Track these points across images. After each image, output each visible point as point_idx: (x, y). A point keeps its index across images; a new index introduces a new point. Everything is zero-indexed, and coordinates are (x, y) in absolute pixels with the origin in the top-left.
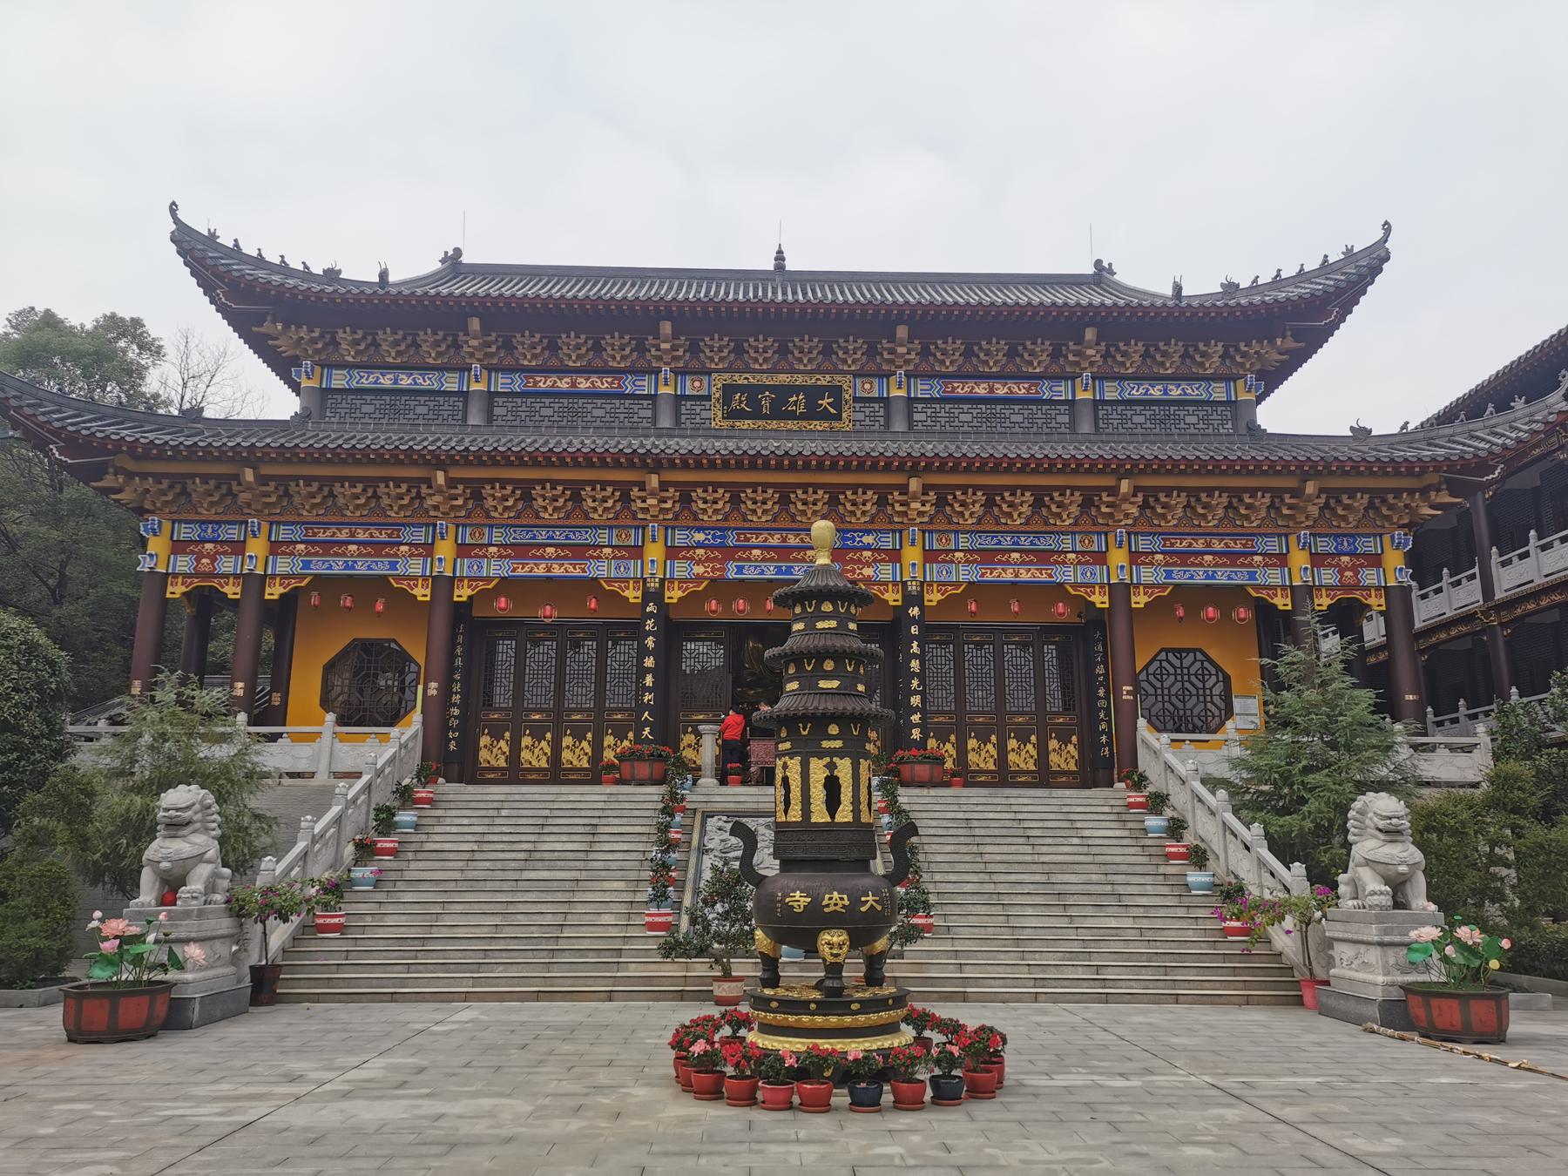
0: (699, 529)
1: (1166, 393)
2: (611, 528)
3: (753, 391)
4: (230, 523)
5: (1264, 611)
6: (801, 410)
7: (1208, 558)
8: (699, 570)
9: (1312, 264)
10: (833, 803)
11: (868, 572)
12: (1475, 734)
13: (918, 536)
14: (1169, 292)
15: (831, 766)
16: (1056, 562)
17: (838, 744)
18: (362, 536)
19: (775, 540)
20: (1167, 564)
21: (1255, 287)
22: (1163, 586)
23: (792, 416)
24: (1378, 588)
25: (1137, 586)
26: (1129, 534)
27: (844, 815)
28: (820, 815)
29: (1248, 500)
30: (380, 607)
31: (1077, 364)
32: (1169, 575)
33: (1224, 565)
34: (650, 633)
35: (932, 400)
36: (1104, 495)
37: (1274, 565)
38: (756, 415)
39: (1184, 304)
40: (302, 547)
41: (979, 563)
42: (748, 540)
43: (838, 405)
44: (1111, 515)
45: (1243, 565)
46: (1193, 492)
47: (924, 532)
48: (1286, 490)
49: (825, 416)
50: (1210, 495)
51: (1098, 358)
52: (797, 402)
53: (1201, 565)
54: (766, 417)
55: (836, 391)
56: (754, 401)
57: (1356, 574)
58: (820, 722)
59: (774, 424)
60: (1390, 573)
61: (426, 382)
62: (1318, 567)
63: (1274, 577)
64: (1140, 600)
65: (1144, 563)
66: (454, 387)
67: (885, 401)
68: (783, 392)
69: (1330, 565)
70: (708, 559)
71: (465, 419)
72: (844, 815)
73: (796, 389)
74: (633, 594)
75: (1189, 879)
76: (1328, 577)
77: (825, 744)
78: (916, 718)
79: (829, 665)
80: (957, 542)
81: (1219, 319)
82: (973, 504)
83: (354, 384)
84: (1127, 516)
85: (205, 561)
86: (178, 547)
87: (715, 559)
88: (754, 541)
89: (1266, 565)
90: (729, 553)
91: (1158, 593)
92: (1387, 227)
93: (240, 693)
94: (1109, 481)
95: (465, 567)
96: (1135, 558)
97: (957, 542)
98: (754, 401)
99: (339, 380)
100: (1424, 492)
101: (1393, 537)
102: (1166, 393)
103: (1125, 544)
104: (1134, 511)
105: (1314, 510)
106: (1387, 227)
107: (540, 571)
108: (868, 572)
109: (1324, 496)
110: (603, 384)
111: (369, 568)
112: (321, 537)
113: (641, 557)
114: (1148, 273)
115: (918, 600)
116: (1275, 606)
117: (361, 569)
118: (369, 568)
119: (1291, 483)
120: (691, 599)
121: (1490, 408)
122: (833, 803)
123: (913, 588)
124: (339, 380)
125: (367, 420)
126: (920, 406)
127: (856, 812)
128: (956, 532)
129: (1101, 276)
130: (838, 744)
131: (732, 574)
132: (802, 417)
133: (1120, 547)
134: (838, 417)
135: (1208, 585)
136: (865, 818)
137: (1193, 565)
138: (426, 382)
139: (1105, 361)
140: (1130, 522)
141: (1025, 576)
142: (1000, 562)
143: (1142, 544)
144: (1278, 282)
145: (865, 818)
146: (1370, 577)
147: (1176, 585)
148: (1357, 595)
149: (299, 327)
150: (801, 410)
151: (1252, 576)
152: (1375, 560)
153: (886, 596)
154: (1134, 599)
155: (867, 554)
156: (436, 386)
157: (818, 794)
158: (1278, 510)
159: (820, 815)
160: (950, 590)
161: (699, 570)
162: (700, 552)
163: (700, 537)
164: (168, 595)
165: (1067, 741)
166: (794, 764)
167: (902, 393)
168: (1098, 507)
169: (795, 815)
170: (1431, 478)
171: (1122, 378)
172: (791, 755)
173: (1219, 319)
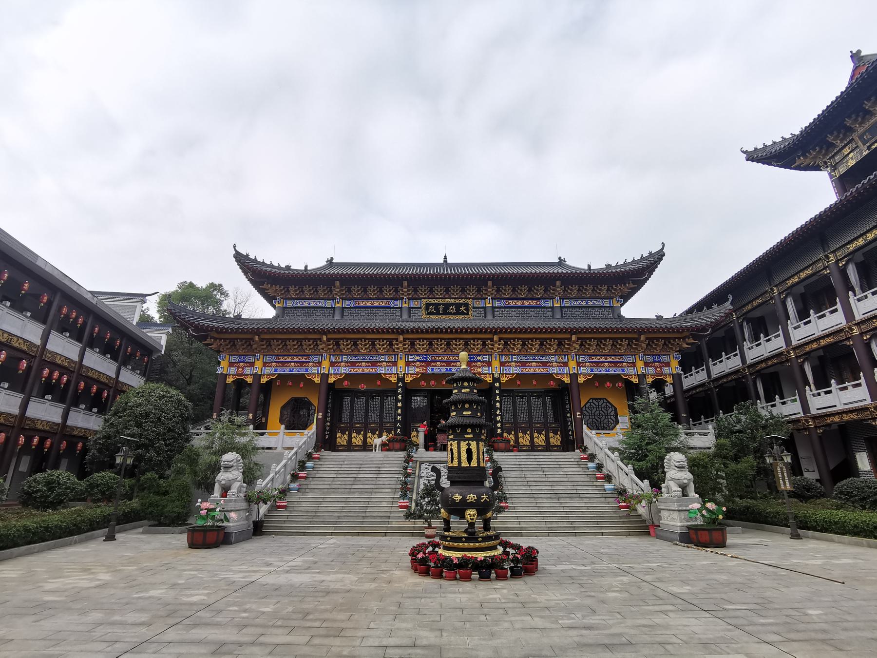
0: (418, 355)
3: (436, 305)
5: (628, 383)
6: (454, 311)
8: (417, 370)
9: (638, 257)
10: (469, 459)
15: (469, 445)
17: (471, 436)
19: (445, 359)
21: (617, 266)
23: (451, 314)
27: (474, 463)
28: (465, 464)
30: (302, 385)
32: (592, 370)
38: (438, 313)
43: (467, 309)
46: (599, 340)
49: (463, 313)
52: (453, 309)
55: (466, 305)
56: (437, 309)
58: (464, 427)
63: (631, 371)
64: (581, 380)
68: (447, 306)
72: (474, 463)
76: (651, 370)
77: (466, 436)
79: (467, 406)
88: (437, 359)
90: (428, 364)
91: (588, 377)
92: (663, 245)
94: (568, 336)
96: (579, 364)
98: (437, 309)
99: (290, 304)
100: (684, 338)
104: (578, 347)
105: (644, 346)
106: (663, 245)
114: (578, 261)
115: (498, 380)
117: (295, 372)
119: (635, 336)
122: (469, 459)
124: (290, 304)
127: (479, 462)
130: (471, 436)
131: (430, 372)
132: (454, 314)
134: (467, 314)
136: (482, 465)
141: (538, 371)
143: (581, 359)
145: (482, 465)
148: (243, 377)
150: (454, 311)
151: (623, 370)
157: (464, 455)
159: (465, 464)
161: (417, 370)
163: (418, 358)
166: (455, 444)
169: (455, 464)
170: (686, 334)
172: (472, 439)
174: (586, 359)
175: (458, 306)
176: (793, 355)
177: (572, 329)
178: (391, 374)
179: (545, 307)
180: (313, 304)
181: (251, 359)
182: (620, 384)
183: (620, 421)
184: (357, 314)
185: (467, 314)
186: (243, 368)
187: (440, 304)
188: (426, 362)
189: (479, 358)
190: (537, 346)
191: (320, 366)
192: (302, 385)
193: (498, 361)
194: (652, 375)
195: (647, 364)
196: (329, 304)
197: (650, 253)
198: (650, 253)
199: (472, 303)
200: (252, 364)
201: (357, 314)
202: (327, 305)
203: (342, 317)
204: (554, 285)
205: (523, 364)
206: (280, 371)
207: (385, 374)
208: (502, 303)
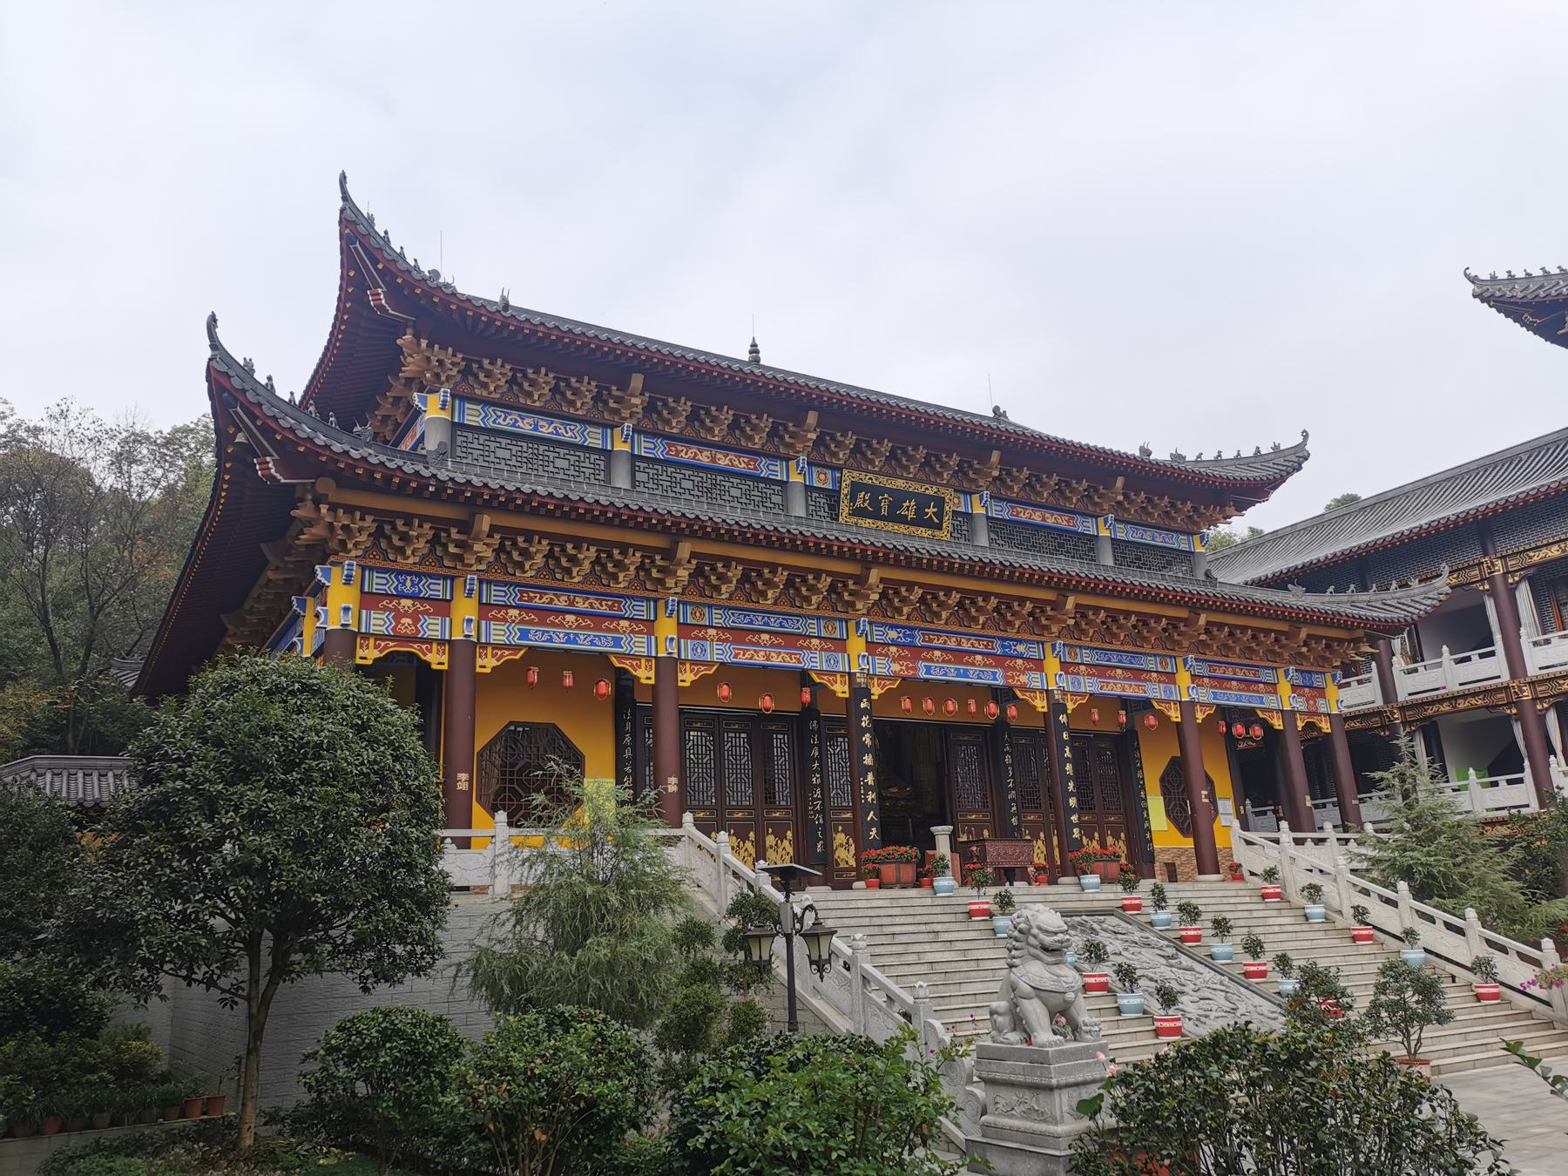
0: (892, 627)
1: (536, 429)
2: (818, 618)
3: (876, 491)
4: (431, 576)
5: (624, 683)
6: (911, 515)
7: (570, 618)
8: (896, 667)
9: (1248, 452)
11: (1023, 679)
12: (680, 825)
13: (356, 572)
14: (745, 356)
16: (802, 648)
18: (581, 605)
19: (952, 644)
20: (522, 622)
21: (1199, 460)
22: (515, 648)
23: (903, 520)
24: (441, 642)
25: (484, 646)
26: (481, 582)
29: (401, 528)
30: (568, 682)
31: (616, 412)
32: (524, 634)
33: (587, 628)
34: (866, 730)
35: (656, 461)
36: (454, 531)
37: (641, 632)
38: (876, 515)
39: (508, 314)
40: (515, 612)
41: (733, 642)
42: (931, 641)
43: (940, 515)
44: (460, 558)
45: (608, 630)
46: (558, 540)
47: (363, 569)
48: (850, 576)
49: (929, 524)
50: (408, 524)
51: (639, 410)
52: (909, 509)
53: (562, 626)
54: (883, 518)
55: (940, 502)
56: (875, 502)
57: (416, 621)
59: (890, 526)
60: (1184, 691)
61: (570, 433)
62: (369, 608)
63: (639, 645)
64: (487, 663)
65: (495, 619)
66: (598, 444)
67: (607, 454)
68: (899, 497)
69: (385, 609)
70: (900, 658)
71: (608, 479)
73: (908, 495)
74: (841, 689)
75: (1215, 950)
76: (379, 622)
78: (1074, 818)
80: (711, 619)
81: (707, 378)
82: (360, 530)
83: (491, 425)
84: (480, 560)
85: (404, 620)
86: (369, 600)
87: (905, 658)
88: (936, 643)
89: (633, 632)
90: (915, 652)
91: (508, 655)
92: (1305, 435)
93: (673, 788)
94: (1183, 613)
95: (688, 650)
96: (485, 609)
97: (711, 619)
98: (875, 502)
99: (473, 415)
101: (858, 624)
102: (536, 429)
103: (475, 594)
104: (489, 554)
105: (683, 574)
106: (1305, 435)
107: (760, 659)
108: (1023, 679)
109: (497, 536)
110: (741, 464)
111: (593, 644)
112: (537, 602)
113: (844, 651)
114: (1365, 493)
115: (866, 693)
116: (834, 692)
117: (583, 645)
118: (928, 672)
119: (1183, 613)
120: (703, 684)
121: (1394, 585)
123: (861, 680)
124: (473, 415)
125: (735, 504)
126: (642, 465)
128: (710, 606)
129: (435, 274)
131: (922, 675)
132: (913, 523)
133: (469, 595)
134: (940, 528)
135: (566, 650)
137: (553, 624)
138: (570, 433)
139: (510, 389)
140: (483, 567)
141: (776, 661)
142: (751, 643)
143: (495, 595)
144: (1218, 460)
146: (433, 627)
147: (530, 647)
148: (414, 648)
149: (444, 348)
150: (911, 515)
151: (617, 642)
152: (442, 607)
153: (429, 658)
154: (479, 662)
155: (1020, 662)
156: (579, 440)
158: (648, 572)
160: (704, 671)
161: (896, 667)
162: (893, 649)
163: (893, 634)
164: (479, 670)
165: (783, 837)
167: (626, 448)
168: (445, 546)
170: (1360, 633)
171: (486, 402)
173: (707, 378)
174: (512, 597)
175: (922, 501)
176: (1527, 695)
177: (477, 493)
178: (1168, 702)
179: (767, 480)
180: (546, 430)
181: (1035, 653)
182: (605, 688)
183: (1221, 810)
184: (674, 483)
185: (940, 528)
186: (415, 615)
187: (883, 490)
188: (911, 646)
189: (1021, 648)
190: (421, 544)
191: (651, 632)
192: (568, 682)
193: (474, 602)
194: (496, 647)
195: (369, 600)
196: (594, 438)
197: (1276, 448)
198: (1276, 448)
199: (955, 503)
200: (442, 607)
201: (674, 483)
202: (590, 442)
203: (634, 486)
204: (624, 385)
205: (738, 635)
206: (538, 639)
207: (820, 673)
208: (660, 450)
